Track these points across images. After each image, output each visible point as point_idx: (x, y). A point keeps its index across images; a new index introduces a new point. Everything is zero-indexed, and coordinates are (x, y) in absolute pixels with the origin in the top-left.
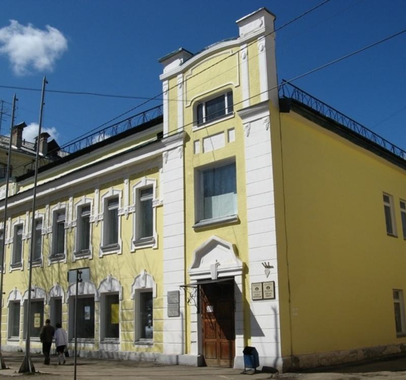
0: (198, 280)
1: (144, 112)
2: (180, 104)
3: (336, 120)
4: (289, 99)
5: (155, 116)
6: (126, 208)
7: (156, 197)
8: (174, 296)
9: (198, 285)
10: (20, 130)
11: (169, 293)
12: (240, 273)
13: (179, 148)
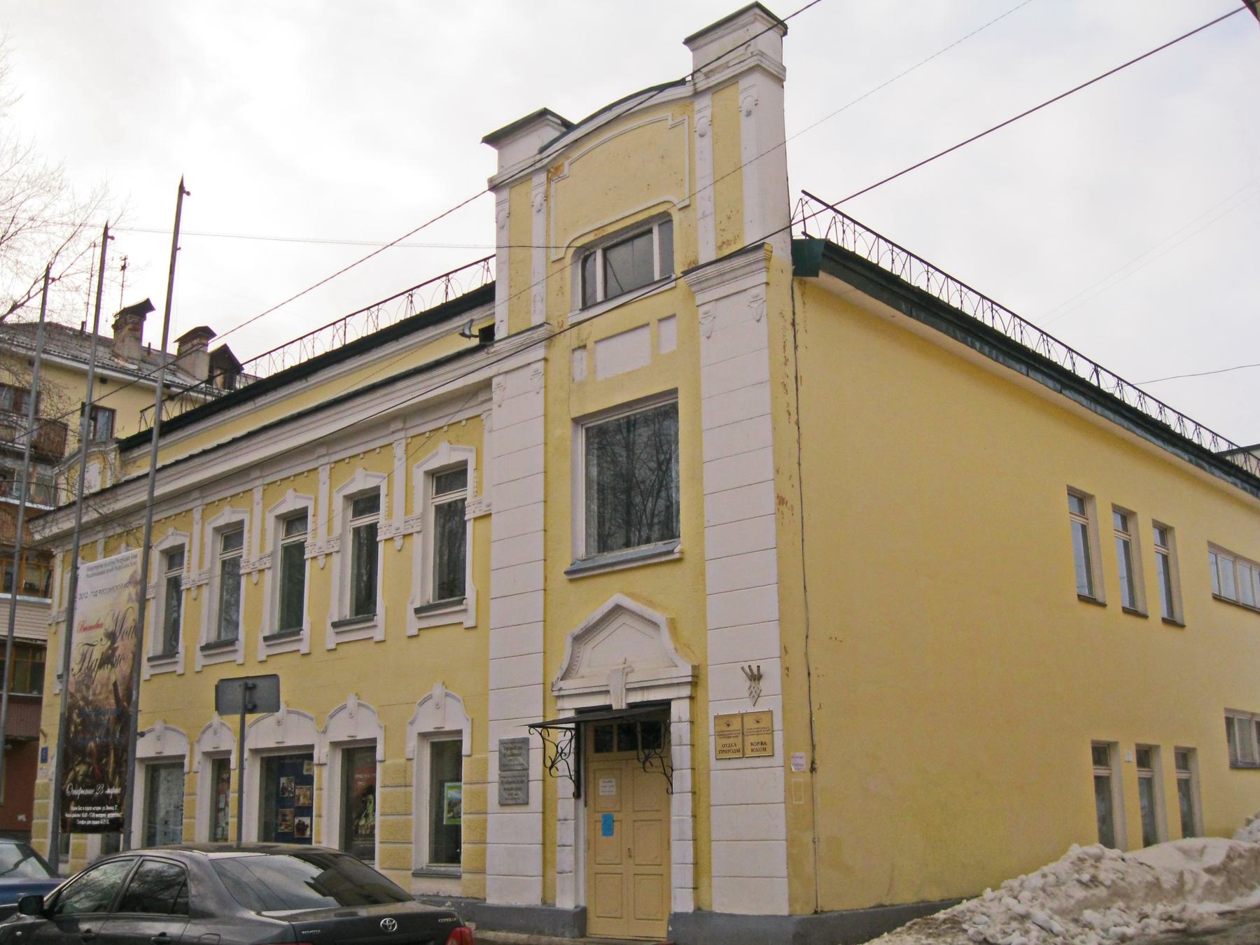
0: (579, 711)
1: (447, 275)
2: (538, 257)
3: (944, 298)
4: (820, 240)
5: (476, 285)
6: (254, 558)
7: (477, 492)
8: (516, 752)
9: (578, 723)
10: (136, 319)
11: (502, 743)
12: (686, 691)
13: (755, 291)
